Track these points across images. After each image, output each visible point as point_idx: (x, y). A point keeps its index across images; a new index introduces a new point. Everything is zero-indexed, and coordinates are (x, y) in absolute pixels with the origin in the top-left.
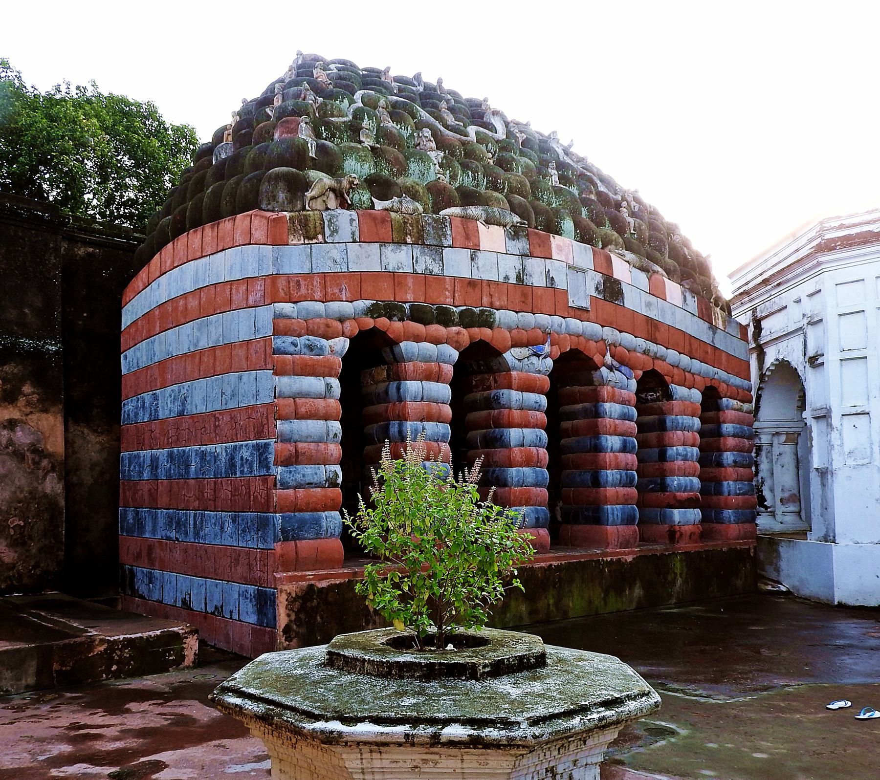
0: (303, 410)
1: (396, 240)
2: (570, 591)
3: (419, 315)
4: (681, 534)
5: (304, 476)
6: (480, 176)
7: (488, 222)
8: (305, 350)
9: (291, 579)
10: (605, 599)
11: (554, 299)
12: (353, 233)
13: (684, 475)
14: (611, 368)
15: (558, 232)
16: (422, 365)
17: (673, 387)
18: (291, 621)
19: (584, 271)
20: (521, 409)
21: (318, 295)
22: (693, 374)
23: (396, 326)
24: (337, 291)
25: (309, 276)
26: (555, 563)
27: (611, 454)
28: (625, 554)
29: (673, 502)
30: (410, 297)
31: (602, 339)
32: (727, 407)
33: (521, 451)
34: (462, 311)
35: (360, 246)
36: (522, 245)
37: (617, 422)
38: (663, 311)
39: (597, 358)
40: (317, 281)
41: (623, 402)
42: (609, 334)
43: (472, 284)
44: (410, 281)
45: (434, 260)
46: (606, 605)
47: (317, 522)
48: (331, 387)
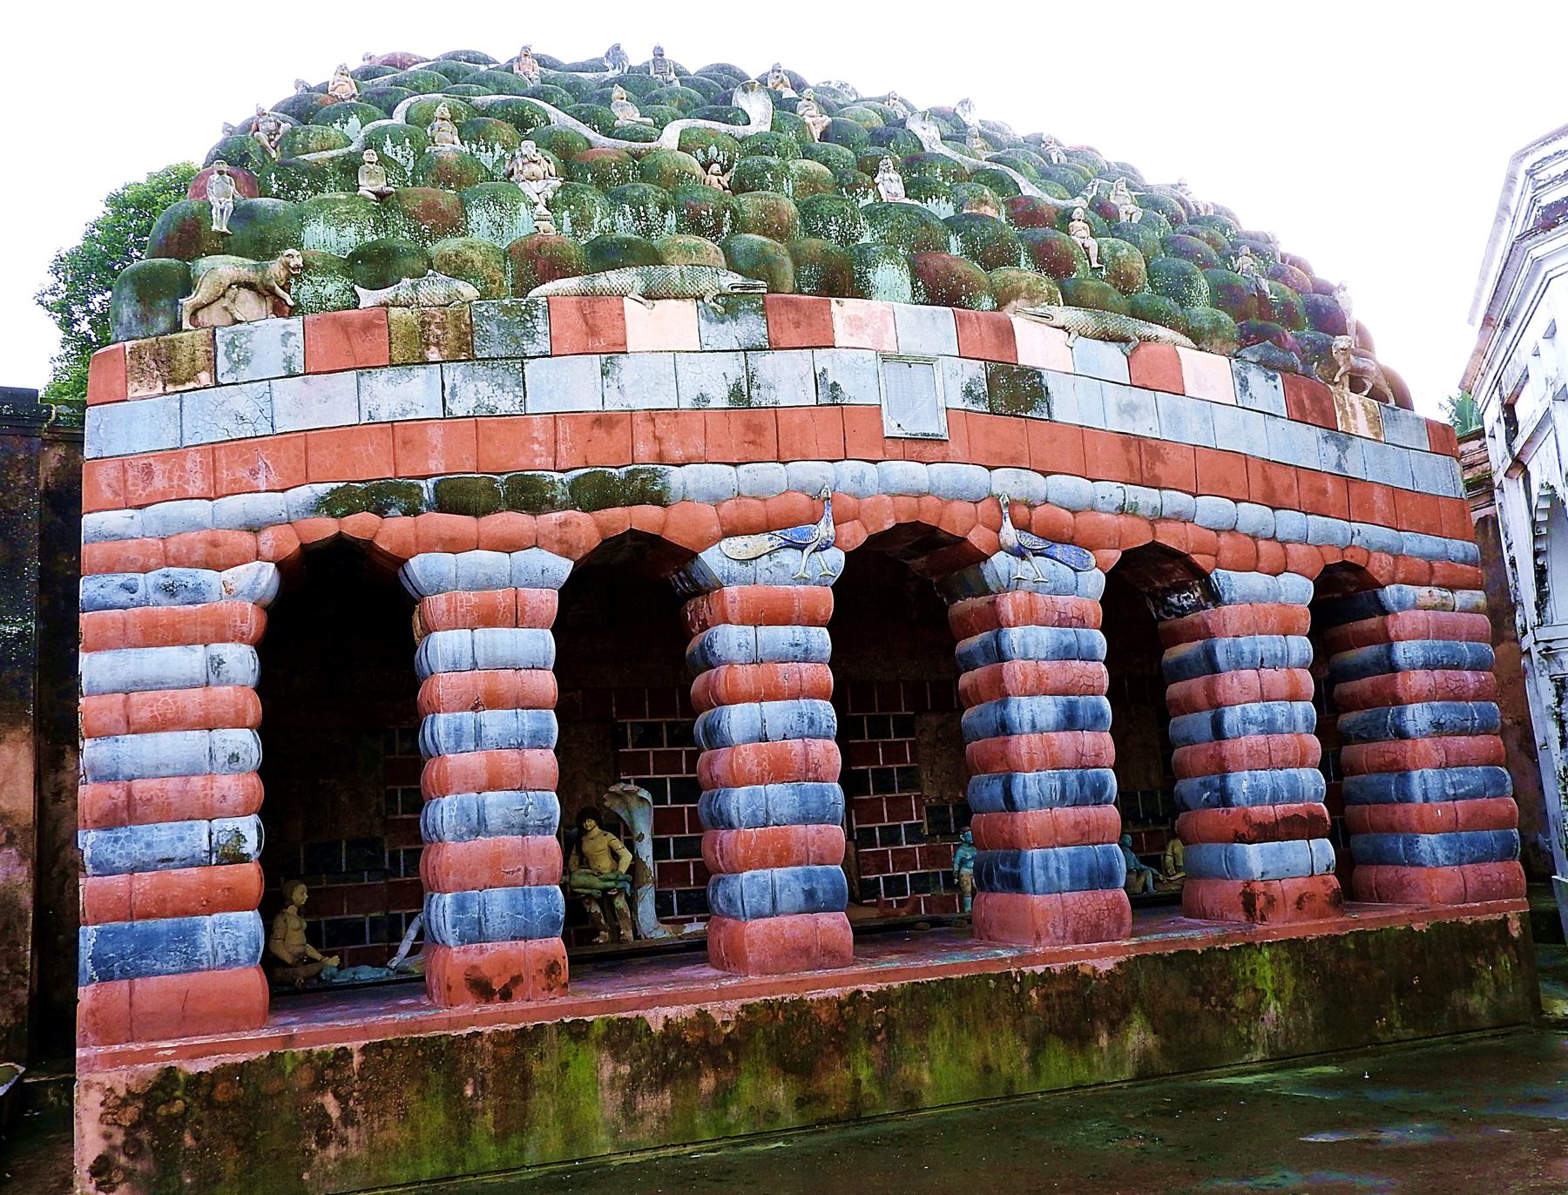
0: (144, 715)
1: (398, 359)
2: (923, 1047)
3: (456, 498)
4: (1271, 901)
5: (149, 845)
6: (653, 209)
7: (650, 295)
8: (159, 596)
9: (114, 1061)
10: (1033, 1058)
11: (845, 425)
12: (289, 360)
13: (1271, 766)
14: (1020, 553)
15: (860, 290)
16: (473, 597)
18: (113, 1148)
19: (928, 361)
20: (757, 662)
21: (197, 485)
22: (1284, 543)
23: (391, 530)
24: (246, 474)
25: (176, 454)
26: (869, 988)
27: (1035, 738)
28: (1089, 954)
29: (1244, 829)
30: (436, 465)
31: (991, 495)
32: (1401, 605)
33: (758, 751)
34: (577, 479)
35: (306, 382)
36: (750, 327)
37: (1045, 666)
38: (1175, 418)
40: (192, 462)
42: (1007, 482)
43: (603, 421)
44: (435, 434)
46: (1037, 1071)
47: (188, 937)
48: (221, 662)
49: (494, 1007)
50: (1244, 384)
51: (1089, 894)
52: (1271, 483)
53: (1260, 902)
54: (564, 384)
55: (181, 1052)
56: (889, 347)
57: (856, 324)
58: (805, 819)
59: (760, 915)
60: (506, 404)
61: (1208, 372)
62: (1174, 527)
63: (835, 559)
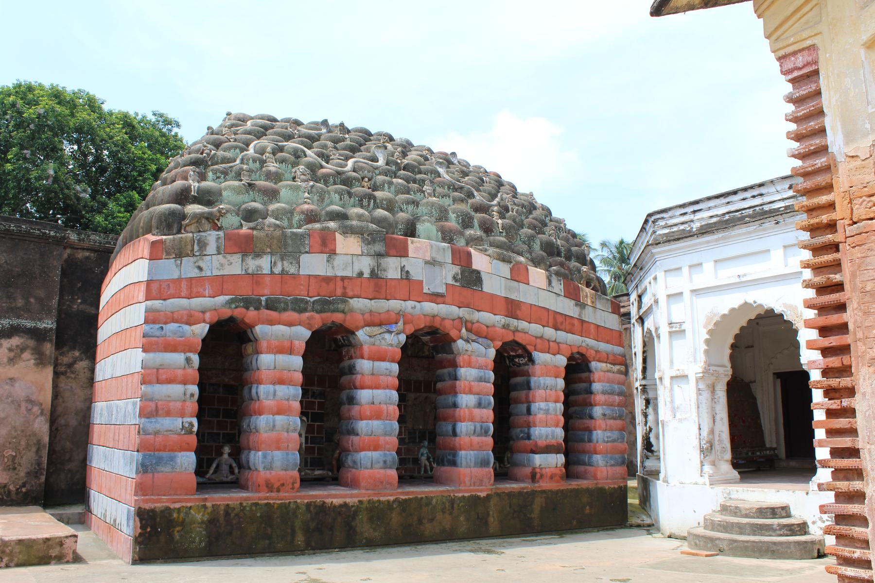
3: (271, 305)
4: (542, 476)
14: (467, 341)
17: (537, 355)
22: (558, 343)
23: (251, 315)
25: (179, 280)
36: (379, 247)
39: (453, 333)
40: (184, 285)
41: (480, 368)
42: (463, 312)
43: (327, 280)
44: (268, 279)
45: (291, 263)
47: (172, 459)
49: (273, 494)
50: (550, 283)
51: (480, 469)
52: (558, 321)
53: (538, 476)
54: (313, 264)
55: (168, 501)
56: (428, 258)
57: (417, 249)
58: (385, 435)
59: (366, 468)
60: (293, 270)
61: (538, 275)
62: (520, 335)
63: (403, 338)
